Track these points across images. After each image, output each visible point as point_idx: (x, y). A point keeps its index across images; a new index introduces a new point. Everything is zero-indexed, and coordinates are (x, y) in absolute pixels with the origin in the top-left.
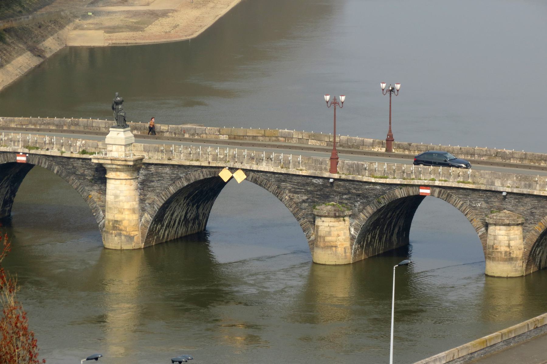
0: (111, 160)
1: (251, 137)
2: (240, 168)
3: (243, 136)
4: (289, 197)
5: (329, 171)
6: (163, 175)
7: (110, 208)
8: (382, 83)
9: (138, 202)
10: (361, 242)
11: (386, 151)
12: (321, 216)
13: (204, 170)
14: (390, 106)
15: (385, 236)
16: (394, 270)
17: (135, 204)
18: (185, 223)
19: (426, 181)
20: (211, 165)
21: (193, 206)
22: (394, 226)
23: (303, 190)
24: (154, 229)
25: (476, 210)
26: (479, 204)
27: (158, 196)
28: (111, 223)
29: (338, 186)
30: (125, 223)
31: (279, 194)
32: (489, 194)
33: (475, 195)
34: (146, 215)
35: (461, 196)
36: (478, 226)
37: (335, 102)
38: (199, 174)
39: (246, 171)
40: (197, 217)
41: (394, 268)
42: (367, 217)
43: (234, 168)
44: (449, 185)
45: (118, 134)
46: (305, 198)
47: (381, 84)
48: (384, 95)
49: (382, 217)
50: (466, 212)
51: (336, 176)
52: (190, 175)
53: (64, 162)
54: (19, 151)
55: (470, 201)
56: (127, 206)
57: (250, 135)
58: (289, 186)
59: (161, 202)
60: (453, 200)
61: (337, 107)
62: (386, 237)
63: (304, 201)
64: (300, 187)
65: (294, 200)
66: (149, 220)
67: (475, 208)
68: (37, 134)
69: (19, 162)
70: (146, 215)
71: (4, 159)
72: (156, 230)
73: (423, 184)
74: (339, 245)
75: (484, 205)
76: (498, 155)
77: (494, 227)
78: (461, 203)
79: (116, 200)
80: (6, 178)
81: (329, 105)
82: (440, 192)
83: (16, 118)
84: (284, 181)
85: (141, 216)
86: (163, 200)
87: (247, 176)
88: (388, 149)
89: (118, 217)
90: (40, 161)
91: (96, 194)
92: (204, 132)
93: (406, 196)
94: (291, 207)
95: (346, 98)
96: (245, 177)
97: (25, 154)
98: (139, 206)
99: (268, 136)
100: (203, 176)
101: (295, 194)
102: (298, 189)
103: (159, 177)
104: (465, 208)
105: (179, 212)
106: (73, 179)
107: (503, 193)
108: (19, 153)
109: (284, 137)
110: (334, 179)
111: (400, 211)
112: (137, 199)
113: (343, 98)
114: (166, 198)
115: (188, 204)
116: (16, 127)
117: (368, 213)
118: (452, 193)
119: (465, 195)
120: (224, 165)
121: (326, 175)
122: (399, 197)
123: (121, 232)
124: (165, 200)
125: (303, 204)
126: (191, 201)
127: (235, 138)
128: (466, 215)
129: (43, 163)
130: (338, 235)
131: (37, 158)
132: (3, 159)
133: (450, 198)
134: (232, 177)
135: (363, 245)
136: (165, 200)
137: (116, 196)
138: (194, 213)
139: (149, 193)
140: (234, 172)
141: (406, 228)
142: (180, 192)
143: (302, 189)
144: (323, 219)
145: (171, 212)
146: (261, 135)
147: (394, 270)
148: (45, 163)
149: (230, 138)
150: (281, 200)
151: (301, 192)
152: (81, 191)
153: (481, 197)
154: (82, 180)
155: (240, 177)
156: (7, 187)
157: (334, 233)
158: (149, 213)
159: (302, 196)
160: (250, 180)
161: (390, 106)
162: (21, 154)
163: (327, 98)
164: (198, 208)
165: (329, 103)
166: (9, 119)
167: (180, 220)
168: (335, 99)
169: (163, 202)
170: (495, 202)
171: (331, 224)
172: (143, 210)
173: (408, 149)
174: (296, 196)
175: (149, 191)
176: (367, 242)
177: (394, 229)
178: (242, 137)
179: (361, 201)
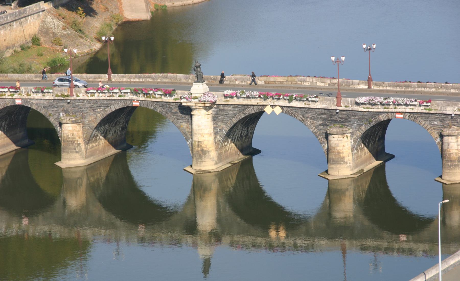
0: (195, 103)
1: (279, 82)
2: (278, 105)
3: (274, 82)
4: (310, 122)
5: (335, 105)
6: (228, 111)
7: (195, 133)
8: (364, 44)
9: (213, 129)
10: (358, 149)
11: (368, 88)
12: (332, 134)
13: (255, 107)
14: (369, 59)
15: (371, 143)
16: (439, 206)
17: (211, 130)
18: (241, 138)
19: (400, 109)
20: (259, 104)
21: (245, 128)
22: (376, 136)
23: (320, 118)
24: (223, 145)
25: (434, 126)
26: (436, 123)
27: (225, 124)
28: (196, 143)
29: (343, 114)
30: (205, 143)
31: (304, 121)
32: (443, 116)
33: (433, 117)
34: (218, 137)
35: (424, 118)
36: (436, 137)
37: (338, 61)
38: (251, 110)
39: (282, 107)
40: (247, 134)
41: (439, 204)
42: (362, 133)
43: (274, 105)
44: (416, 112)
45: (199, 86)
46: (321, 122)
47: (363, 45)
48: (365, 52)
49: (370, 132)
50: (428, 128)
51: (340, 108)
52: (246, 111)
53: (164, 105)
54: (134, 99)
55: (430, 121)
56: (206, 132)
57: (279, 80)
58: (310, 116)
59: (228, 129)
60: (419, 121)
61: (340, 64)
62: (372, 143)
63: (320, 125)
64: (318, 116)
65: (314, 124)
66: (220, 140)
67: (433, 125)
68: (35, 11)
69: (134, 106)
70: (218, 137)
71: (124, 104)
72: (224, 146)
73: (398, 111)
74: (345, 152)
75: (440, 123)
76: (442, 87)
77: (447, 137)
78: (424, 122)
79: (199, 128)
80: (123, 114)
81: (334, 63)
82: (409, 116)
83: (127, 74)
84: (306, 113)
85: (215, 138)
86: (229, 127)
87: (283, 110)
88: (369, 87)
89: (201, 139)
90: (148, 105)
91: (185, 124)
92: (249, 80)
93: (387, 119)
94: (312, 128)
95: (345, 58)
96: (282, 111)
97: (138, 100)
98: (214, 131)
99: (290, 81)
100: (254, 111)
101: (314, 121)
102: (316, 117)
103: (225, 112)
104: (426, 126)
105: (238, 132)
106: (170, 116)
107: (452, 115)
108: (134, 100)
109: (300, 81)
110: (339, 110)
111: (380, 127)
112: (212, 127)
113: (343, 59)
114: (230, 126)
115: (243, 128)
116: (126, 80)
117: (362, 131)
118: (418, 116)
119: (426, 117)
120: (268, 104)
121: (335, 107)
122: (383, 120)
123: (203, 148)
124: (230, 127)
125: (320, 126)
126: (244, 125)
127: (269, 83)
128: (427, 130)
129: (150, 106)
130: (344, 146)
131: (146, 103)
132: (124, 104)
133: (416, 120)
134: (273, 110)
135: (359, 151)
136: (230, 127)
137: (199, 126)
138: (246, 132)
139: (220, 123)
140: (274, 108)
141: (383, 136)
142: (239, 122)
143: (319, 117)
144: (333, 136)
145: (233, 133)
146: (286, 80)
147: (439, 206)
148: (151, 106)
149: (265, 83)
150: (305, 125)
151: (318, 119)
152: (176, 123)
153: (437, 118)
154: (176, 116)
155: (278, 111)
156: (124, 119)
157: (341, 144)
158: (220, 136)
159: (319, 122)
160: (285, 112)
161: (369, 59)
162: (136, 101)
163: (333, 59)
164: (248, 129)
165: (334, 63)
166: (122, 76)
167: (238, 138)
168: (338, 59)
169: (229, 128)
170: (447, 121)
171: (339, 139)
172: (216, 134)
173: (382, 86)
174: (315, 121)
175: (220, 122)
176: (361, 148)
177: (376, 139)
178: (273, 82)
179: (358, 123)
